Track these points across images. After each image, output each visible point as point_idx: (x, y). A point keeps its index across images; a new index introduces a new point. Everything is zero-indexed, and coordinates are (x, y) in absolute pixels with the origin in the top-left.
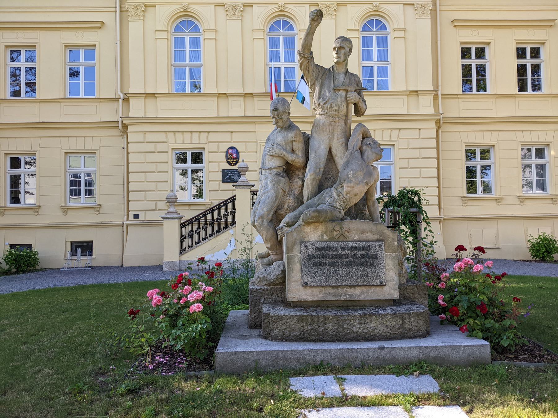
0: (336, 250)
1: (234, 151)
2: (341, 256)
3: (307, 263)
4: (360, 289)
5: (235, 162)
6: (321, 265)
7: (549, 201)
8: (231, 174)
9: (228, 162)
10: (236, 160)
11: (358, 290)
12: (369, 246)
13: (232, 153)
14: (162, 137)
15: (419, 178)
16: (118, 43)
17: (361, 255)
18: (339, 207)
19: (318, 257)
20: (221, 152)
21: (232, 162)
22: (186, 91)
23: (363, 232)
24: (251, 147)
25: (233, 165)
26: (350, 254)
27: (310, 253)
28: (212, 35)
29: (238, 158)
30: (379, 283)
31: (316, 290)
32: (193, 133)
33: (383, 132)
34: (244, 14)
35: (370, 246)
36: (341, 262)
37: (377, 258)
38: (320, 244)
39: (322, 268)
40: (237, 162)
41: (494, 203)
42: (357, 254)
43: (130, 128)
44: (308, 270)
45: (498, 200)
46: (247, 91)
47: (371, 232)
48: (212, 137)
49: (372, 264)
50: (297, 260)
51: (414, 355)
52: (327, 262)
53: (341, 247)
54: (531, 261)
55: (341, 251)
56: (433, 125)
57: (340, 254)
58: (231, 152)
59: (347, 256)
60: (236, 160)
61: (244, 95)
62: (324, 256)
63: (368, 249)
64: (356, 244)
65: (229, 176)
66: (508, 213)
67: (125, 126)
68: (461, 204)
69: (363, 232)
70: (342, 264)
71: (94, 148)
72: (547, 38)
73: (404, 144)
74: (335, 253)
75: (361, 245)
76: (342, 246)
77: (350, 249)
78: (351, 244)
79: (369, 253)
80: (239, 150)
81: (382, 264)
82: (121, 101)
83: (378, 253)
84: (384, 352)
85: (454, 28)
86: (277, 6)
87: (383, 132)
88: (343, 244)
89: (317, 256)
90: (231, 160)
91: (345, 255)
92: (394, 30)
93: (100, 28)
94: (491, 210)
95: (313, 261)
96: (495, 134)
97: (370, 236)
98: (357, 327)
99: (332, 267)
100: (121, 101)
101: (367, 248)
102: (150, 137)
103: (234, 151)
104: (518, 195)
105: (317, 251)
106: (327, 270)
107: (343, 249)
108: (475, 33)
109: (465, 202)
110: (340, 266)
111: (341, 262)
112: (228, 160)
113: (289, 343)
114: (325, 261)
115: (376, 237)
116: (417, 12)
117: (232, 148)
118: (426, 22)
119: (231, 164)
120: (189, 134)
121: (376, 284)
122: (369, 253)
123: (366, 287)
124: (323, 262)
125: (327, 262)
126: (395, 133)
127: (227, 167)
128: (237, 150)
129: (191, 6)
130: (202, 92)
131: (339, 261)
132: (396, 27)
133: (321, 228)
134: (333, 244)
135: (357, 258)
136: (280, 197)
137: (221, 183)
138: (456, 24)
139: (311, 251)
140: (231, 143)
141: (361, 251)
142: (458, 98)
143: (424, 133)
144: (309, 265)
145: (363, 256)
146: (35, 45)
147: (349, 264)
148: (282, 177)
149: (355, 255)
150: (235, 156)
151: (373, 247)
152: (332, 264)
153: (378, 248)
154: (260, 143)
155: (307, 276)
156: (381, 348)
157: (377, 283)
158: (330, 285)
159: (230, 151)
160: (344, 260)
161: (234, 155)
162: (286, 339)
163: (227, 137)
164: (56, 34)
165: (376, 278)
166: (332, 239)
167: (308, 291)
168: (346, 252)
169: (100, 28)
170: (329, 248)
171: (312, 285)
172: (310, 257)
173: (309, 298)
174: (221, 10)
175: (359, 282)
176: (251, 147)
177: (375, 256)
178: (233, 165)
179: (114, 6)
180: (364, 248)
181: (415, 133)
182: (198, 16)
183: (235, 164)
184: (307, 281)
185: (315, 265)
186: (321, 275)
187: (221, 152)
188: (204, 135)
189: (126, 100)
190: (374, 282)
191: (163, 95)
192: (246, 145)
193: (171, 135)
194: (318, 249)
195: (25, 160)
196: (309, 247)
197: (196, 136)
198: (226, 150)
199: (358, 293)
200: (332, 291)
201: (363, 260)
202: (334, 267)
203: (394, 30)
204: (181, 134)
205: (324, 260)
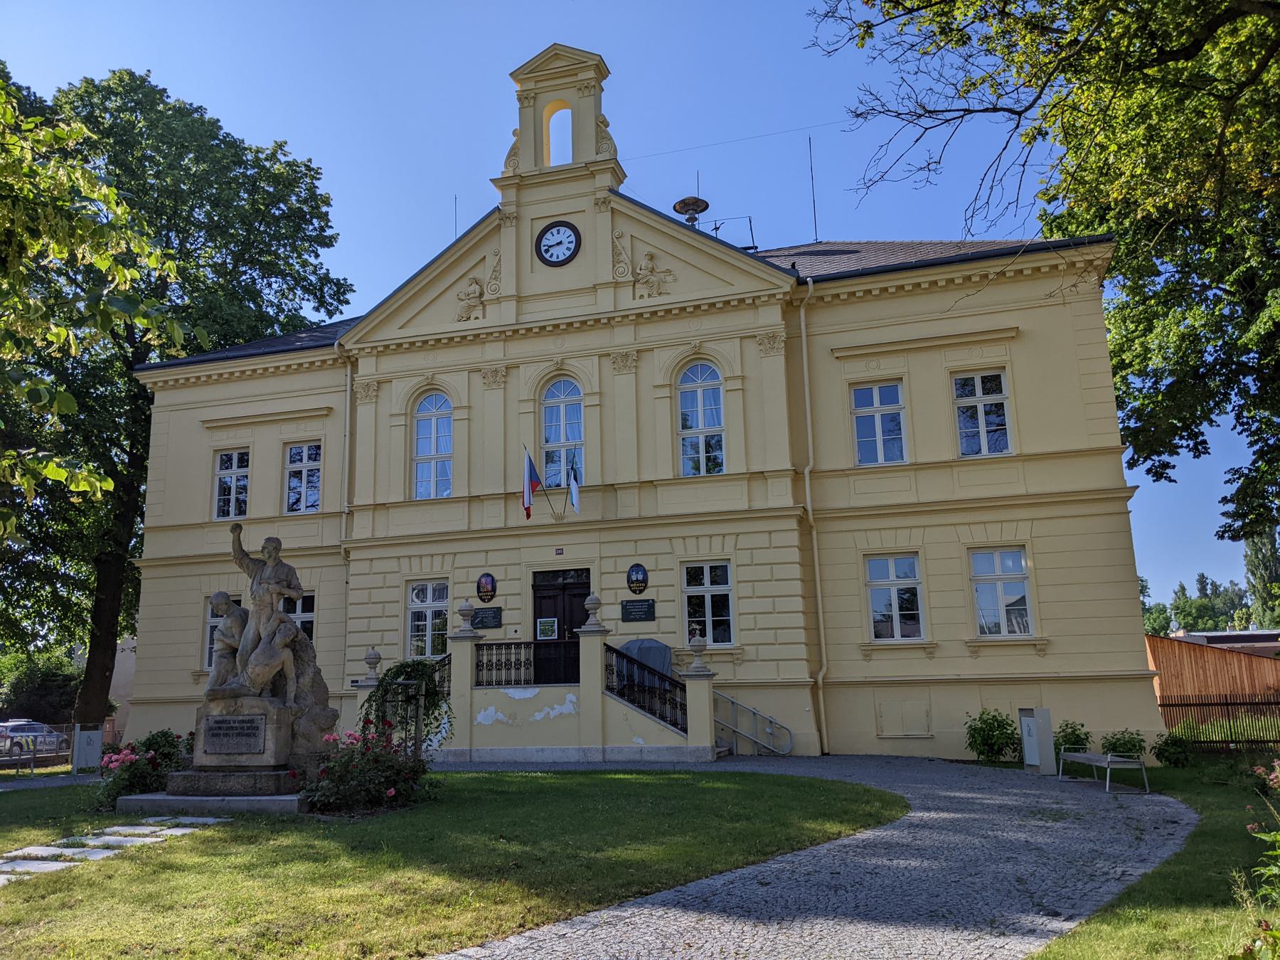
2: (232, 728)
6: (217, 735)
7: (1032, 651)
11: (244, 757)
14: (392, 565)
15: (771, 613)
16: (347, 434)
23: (252, 707)
24: (513, 572)
28: (463, 414)
29: (494, 589)
31: (214, 757)
33: (685, 543)
34: (508, 379)
38: (221, 718)
40: (493, 597)
41: (921, 654)
43: (353, 555)
45: (930, 650)
46: (510, 490)
47: (258, 707)
48: (461, 560)
49: (254, 735)
50: (202, 731)
51: (244, 806)
54: (973, 762)
56: (793, 524)
59: (236, 728)
60: (492, 593)
62: (220, 728)
66: (949, 673)
67: (347, 552)
68: (862, 657)
69: (252, 707)
71: (914, 544)
72: (1007, 358)
73: (744, 557)
77: (239, 722)
78: (241, 718)
80: (496, 578)
82: (344, 516)
84: (224, 803)
85: (837, 362)
86: (552, 363)
87: (685, 543)
88: (235, 718)
92: (726, 379)
93: (327, 415)
94: (917, 667)
96: (917, 533)
97: (257, 711)
98: (220, 785)
100: (344, 516)
101: (252, 721)
102: (378, 566)
103: (489, 579)
104: (967, 639)
107: (234, 722)
108: (873, 364)
109: (868, 652)
115: (262, 711)
116: (761, 347)
117: (488, 575)
118: (777, 362)
119: (483, 600)
120: (429, 558)
126: (730, 541)
127: (478, 604)
128: (493, 578)
129: (437, 376)
132: (728, 375)
133: (222, 704)
134: (228, 718)
138: (836, 355)
139: (212, 724)
142: (848, 476)
143: (778, 539)
145: (248, 728)
147: (238, 735)
149: (220, 728)
150: (489, 587)
152: (226, 735)
156: (223, 800)
162: (174, 794)
163: (479, 559)
164: (273, 429)
166: (228, 714)
167: (209, 757)
168: (237, 725)
169: (327, 415)
170: (223, 722)
172: (211, 729)
173: (208, 763)
174: (476, 378)
175: (244, 750)
176: (513, 572)
179: (344, 383)
180: (249, 721)
181: (763, 540)
183: (489, 600)
185: (213, 735)
188: (449, 559)
189: (350, 513)
191: (396, 505)
193: (405, 562)
194: (217, 722)
197: (415, 561)
199: (244, 760)
200: (225, 757)
203: (726, 379)
204: (407, 560)
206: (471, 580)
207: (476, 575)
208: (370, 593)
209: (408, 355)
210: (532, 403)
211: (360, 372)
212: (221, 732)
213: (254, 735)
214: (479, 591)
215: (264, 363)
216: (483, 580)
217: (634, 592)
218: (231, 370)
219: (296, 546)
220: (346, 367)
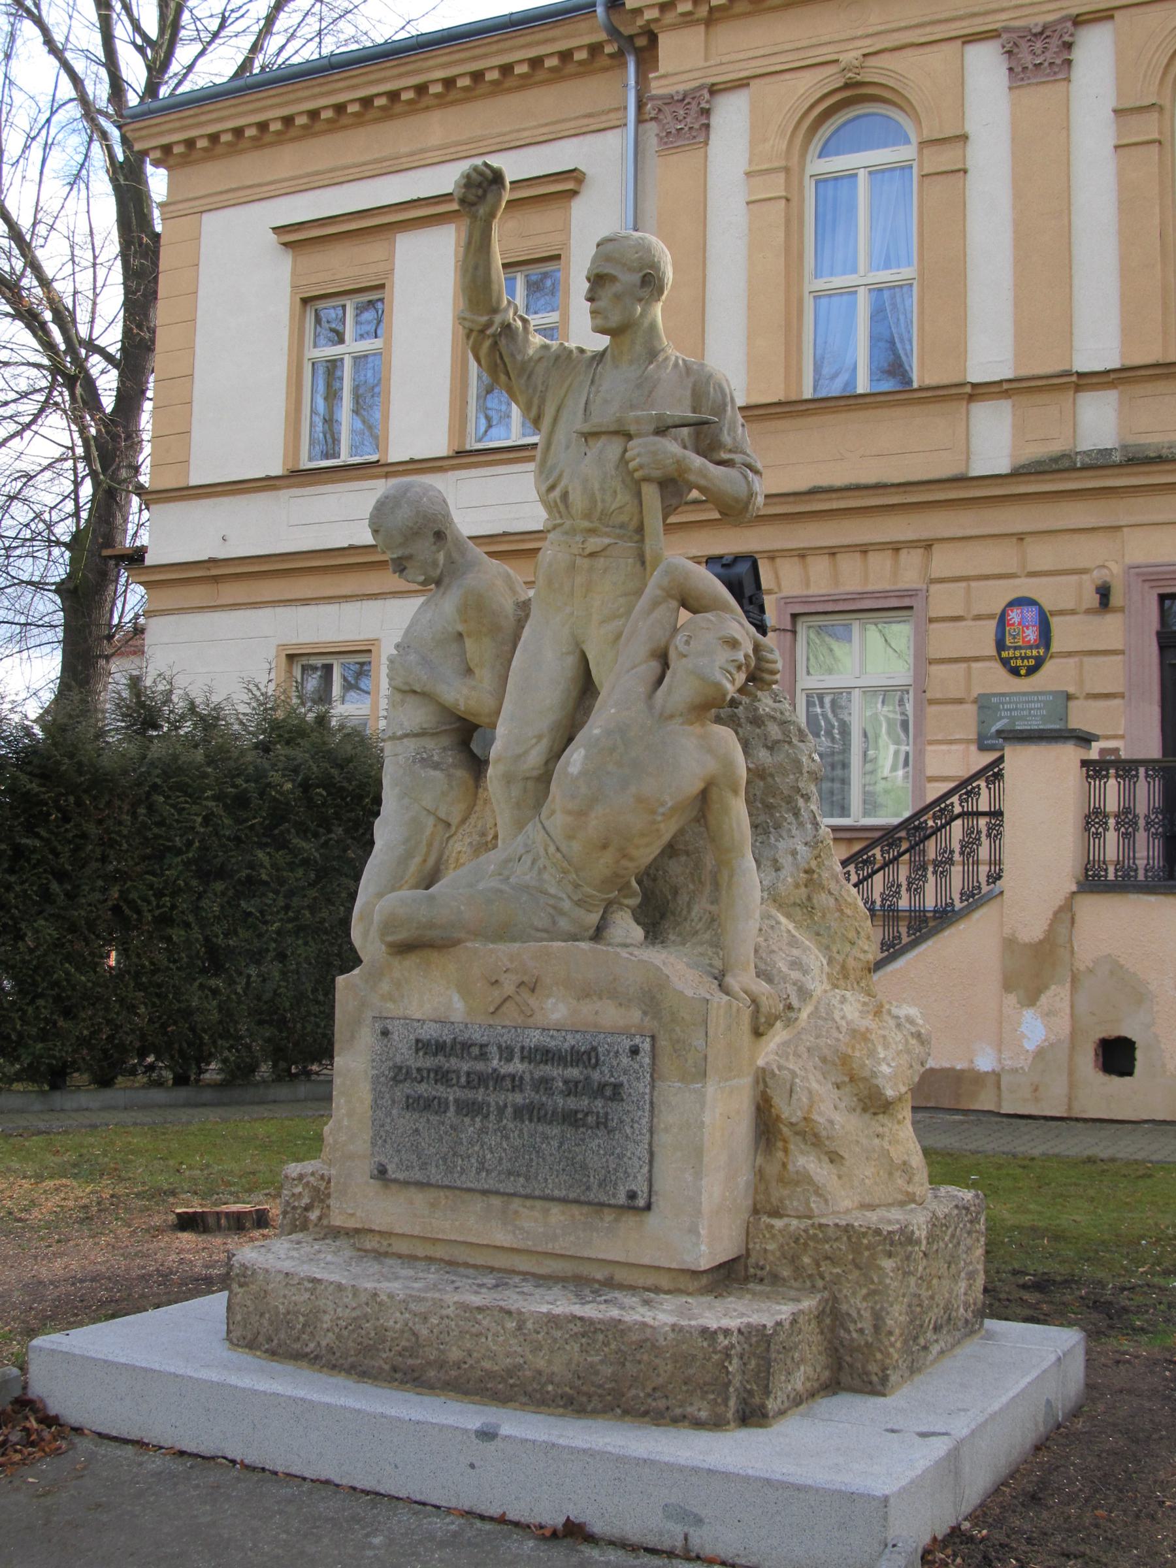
0: (483, 1056)
1: (1031, 614)
2: (498, 1079)
3: (387, 1096)
4: (563, 1213)
5: (1032, 662)
6: (425, 1105)
8: (1015, 713)
9: (1005, 662)
10: (1035, 653)
12: (594, 1049)
13: (1020, 624)
17: (566, 1082)
18: (552, 891)
19: (422, 1076)
20: (978, 618)
21: (1019, 662)
22: (910, 382)
25: (1023, 672)
26: (527, 1077)
27: (398, 1059)
30: (622, 1199)
32: (936, 548)
35: (600, 1049)
36: (497, 1103)
37: (622, 1100)
39: (434, 1119)
40: (1039, 664)
42: (553, 1079)
44: (388, 1120)
49: (603, 1123)
52: (451, 1098)
53: (500, 1047)
55: (500, 1060)
57: (495, 1070)
58: (1016, 620)
59: (516, 1083)
61: (1074, 379)
62: (443, 1076)
63: (590, 1059)
64: (552, 1037)
65: (1006, 721)
70: (501, 1110)
74: (480, 1066)
75: (566, 1046)
76: (502, 1040)
79: (596, 1076)
81: (636, 1125)
83: (624, 1079)
89: (419, 1070)
90: (1017, 654)
91: (513, 1077)
95: (407, 1088)
99: (467, 1120)
101: (586, 1057)
103: (1031, 614)
105: (421, 1054)
106: (451, 1127)
110: (492, 1117)
111: (497, 1103)
112: (1004, 654)
113: (367, 1387)
114: (445, 1095)
121: (612, 1202)
122: (596, 1076)
123: (585, 1209)
124: (439, 1098)
125: (451, 1098)
129: (872, 62)
130: (915, 385)
131: (491, 1099)
135: (549, 1091)
136: (430, 845)
137: (973, 748)
139: (405, 1055)
140: (1017, 581)
141: (565, 1066)
144: (394, 1102)
145: (573, 1088)
146: (557, 252)
148: (436, 766)
149: (544, 1084)
150: (1032, 635)
151: (609, 1052)
152: (469, 1109)
153: (625, 1060)
154: (1138, 574)
155: (385, 1141)
157: (614, 1195)
158: (458, 1183)
159: (1014, 616)
160: (507, 1097)
161: (1028, 632)
165: (613, 1178)
168: (517, 1066)
170: (462, 1048)
171: (401, 1176)
172: (400, 1075)
177: (615, 1092)
178: (1023, 672)
182: (892, 89)
184: (385, 1161)
186: (430, 1145)
187: (978, 618)
190: (607, 1193)
192: (968, 590)
194: (422, 1046)
195: (1088, 611)
196: (395, 1037)
198: (999, 611)
201: (572, 1103)
202: (473, 1119)
205: (441, 1091)
206: (984, 609)
207: (995, 597)
208: (968, 589)
209: (338, 138)
210: (782, 177)
211: (664, 66)
212: (451, 1094)
213: (603, 1123)
214: (1000, 645)
215: (474, 58)
216: (1014, 616)
217: (1015, 672)
218: (165, 140)
219: (802, 485)
220: (624, 65)
